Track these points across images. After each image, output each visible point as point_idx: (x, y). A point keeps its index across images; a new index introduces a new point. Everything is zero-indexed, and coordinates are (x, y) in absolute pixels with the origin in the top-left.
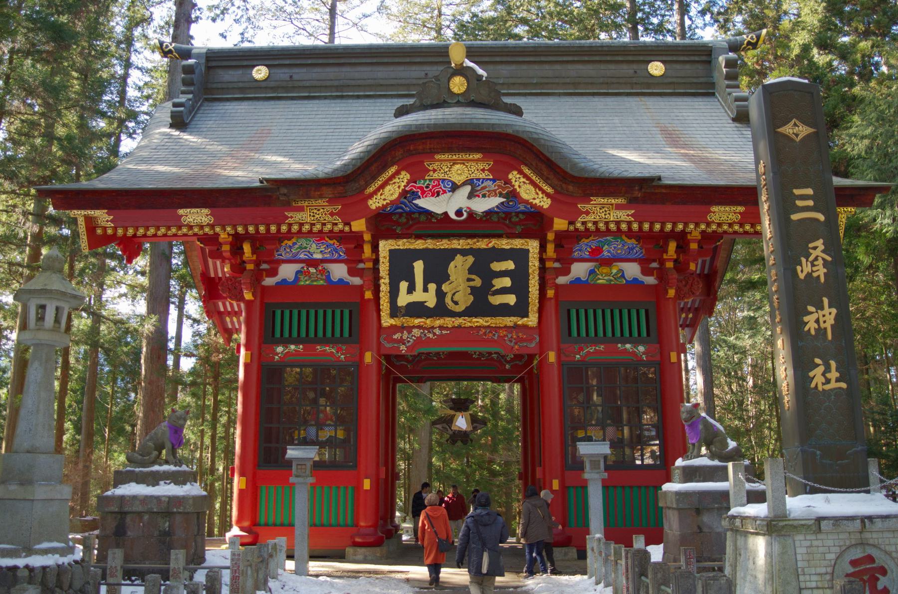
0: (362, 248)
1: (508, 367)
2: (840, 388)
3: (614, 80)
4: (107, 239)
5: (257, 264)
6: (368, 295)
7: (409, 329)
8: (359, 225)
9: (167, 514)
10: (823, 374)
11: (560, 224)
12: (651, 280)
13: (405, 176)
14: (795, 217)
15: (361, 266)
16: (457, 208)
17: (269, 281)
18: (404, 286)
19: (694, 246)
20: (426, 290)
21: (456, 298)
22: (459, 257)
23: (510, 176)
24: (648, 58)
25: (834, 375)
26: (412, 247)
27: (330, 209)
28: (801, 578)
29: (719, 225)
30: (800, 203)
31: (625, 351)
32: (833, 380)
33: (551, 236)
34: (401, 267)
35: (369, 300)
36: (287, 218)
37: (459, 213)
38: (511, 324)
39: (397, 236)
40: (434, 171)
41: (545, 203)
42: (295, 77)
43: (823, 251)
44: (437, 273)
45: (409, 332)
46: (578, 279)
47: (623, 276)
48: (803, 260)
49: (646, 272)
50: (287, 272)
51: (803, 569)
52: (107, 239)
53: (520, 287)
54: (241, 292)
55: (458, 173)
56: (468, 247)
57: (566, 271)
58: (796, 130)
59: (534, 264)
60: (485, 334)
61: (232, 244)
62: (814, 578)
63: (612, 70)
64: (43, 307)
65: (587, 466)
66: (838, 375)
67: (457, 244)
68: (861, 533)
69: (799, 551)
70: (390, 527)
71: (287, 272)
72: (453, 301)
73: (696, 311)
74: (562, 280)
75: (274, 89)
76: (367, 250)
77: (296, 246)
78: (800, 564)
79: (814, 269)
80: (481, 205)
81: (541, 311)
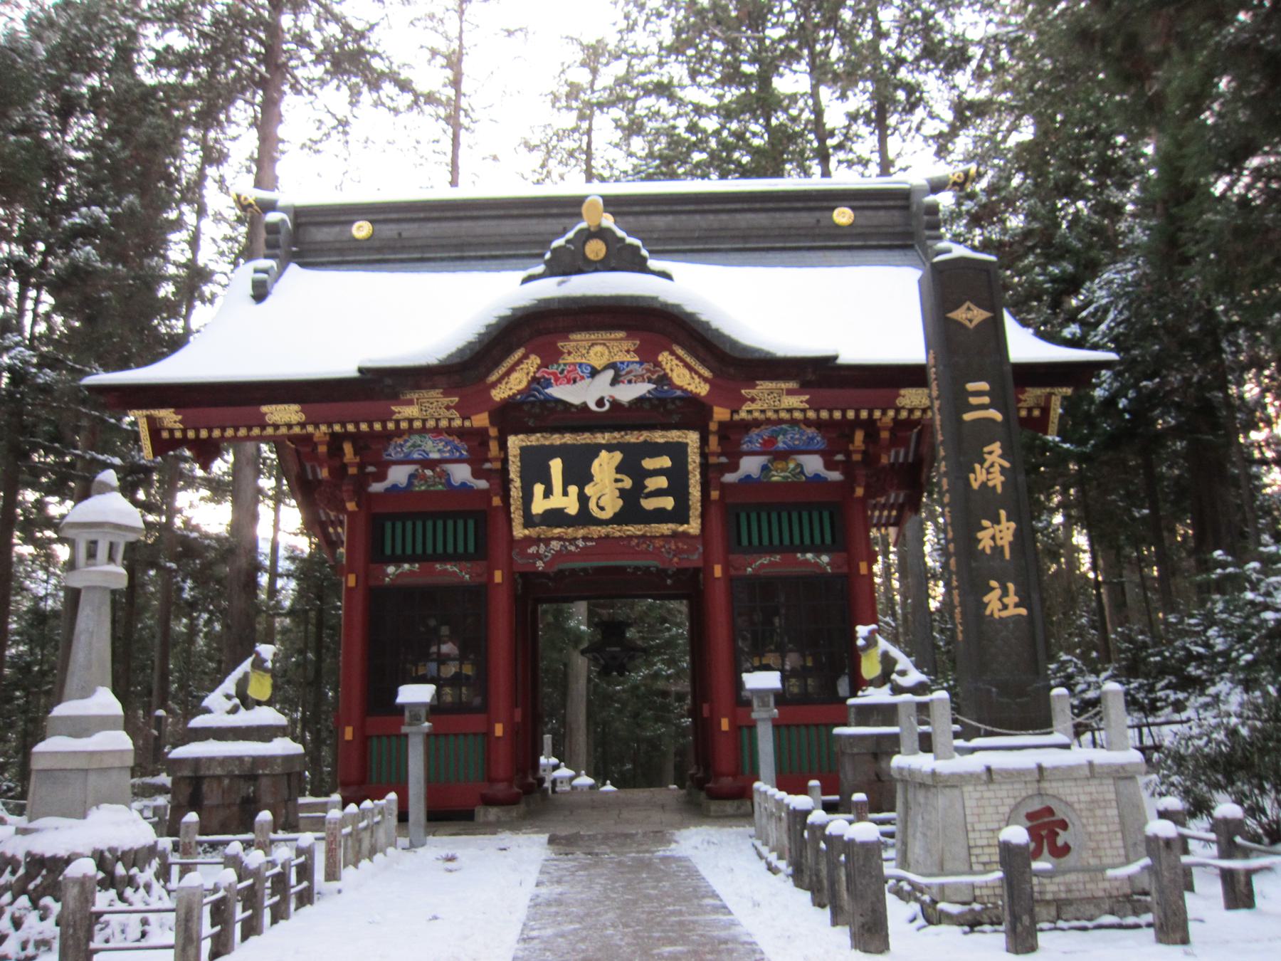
0: (488, 446)
1: (669, 582)
2: (1019, 615)
3: (793, 232)
4: (175, 444)
5: (361, 466)
6: (496, 501)
7: (547, 541)
8: (481, 420)
9: (252, 777)
10: (1000, 599)
11: (721, 414)
12: (835, 476)
13: (534, 360)
14: (968, 417)
15: (487, 466)
16: (597, 397)
17: (377, 487)
18: (539, 489)
19: (885, 435)
20: (565, 493)
21: (602, 503)
22: (604, 454)
23: (660, 358)
24: (833, 204)
25: (1012, 599)
26: (547, 443)
27: (446, 401)
28: (971, 835)
29: (911, 411)
30: (974, 401)
31: (807, 562)
32: (1011, 606)
33: (713, 426)
34: (535, 470)
35: (497, 507)
36: (394, 413)
37: (600, 403)
38: (669, 533)
39: (529, 431)
40: (569, 353)
41: (702, 389)
42: (405, 234)
43: (1001, 456)
44: (578, 474)
45: (547, 545)
46: (748, 477)
47: (802, 472)
48: (977, 466)
49: (829, 465)
50: (398, 475)
51: (973, 824)
52: (175, 444)
53: (678, 487)
54: (343, 502)
55: (598, 356)
56: (615, 441)
57: (734, 467)
58: (969, 315)
59: (694, 459)
60: (638, 545)
61: (329, 445)
62: (985, 834)
63: (789, 219)
64: (95, 543)
65: (755, 703)
66: (1016, 599)
67: (601, 438)
68: (1039, 781)
69: (968, 803)
70: (531, 780)
71: (398, 475)
72: (598, 506)
73: (901, 508)
74: (729, 478)
75: (379, 250)
76: (494, 447)
77: (409, 444)
78: (969, 819)
79: (990, 476)
80: (628, 393)
81: (703, 516)
